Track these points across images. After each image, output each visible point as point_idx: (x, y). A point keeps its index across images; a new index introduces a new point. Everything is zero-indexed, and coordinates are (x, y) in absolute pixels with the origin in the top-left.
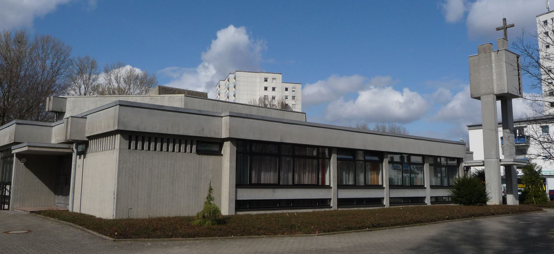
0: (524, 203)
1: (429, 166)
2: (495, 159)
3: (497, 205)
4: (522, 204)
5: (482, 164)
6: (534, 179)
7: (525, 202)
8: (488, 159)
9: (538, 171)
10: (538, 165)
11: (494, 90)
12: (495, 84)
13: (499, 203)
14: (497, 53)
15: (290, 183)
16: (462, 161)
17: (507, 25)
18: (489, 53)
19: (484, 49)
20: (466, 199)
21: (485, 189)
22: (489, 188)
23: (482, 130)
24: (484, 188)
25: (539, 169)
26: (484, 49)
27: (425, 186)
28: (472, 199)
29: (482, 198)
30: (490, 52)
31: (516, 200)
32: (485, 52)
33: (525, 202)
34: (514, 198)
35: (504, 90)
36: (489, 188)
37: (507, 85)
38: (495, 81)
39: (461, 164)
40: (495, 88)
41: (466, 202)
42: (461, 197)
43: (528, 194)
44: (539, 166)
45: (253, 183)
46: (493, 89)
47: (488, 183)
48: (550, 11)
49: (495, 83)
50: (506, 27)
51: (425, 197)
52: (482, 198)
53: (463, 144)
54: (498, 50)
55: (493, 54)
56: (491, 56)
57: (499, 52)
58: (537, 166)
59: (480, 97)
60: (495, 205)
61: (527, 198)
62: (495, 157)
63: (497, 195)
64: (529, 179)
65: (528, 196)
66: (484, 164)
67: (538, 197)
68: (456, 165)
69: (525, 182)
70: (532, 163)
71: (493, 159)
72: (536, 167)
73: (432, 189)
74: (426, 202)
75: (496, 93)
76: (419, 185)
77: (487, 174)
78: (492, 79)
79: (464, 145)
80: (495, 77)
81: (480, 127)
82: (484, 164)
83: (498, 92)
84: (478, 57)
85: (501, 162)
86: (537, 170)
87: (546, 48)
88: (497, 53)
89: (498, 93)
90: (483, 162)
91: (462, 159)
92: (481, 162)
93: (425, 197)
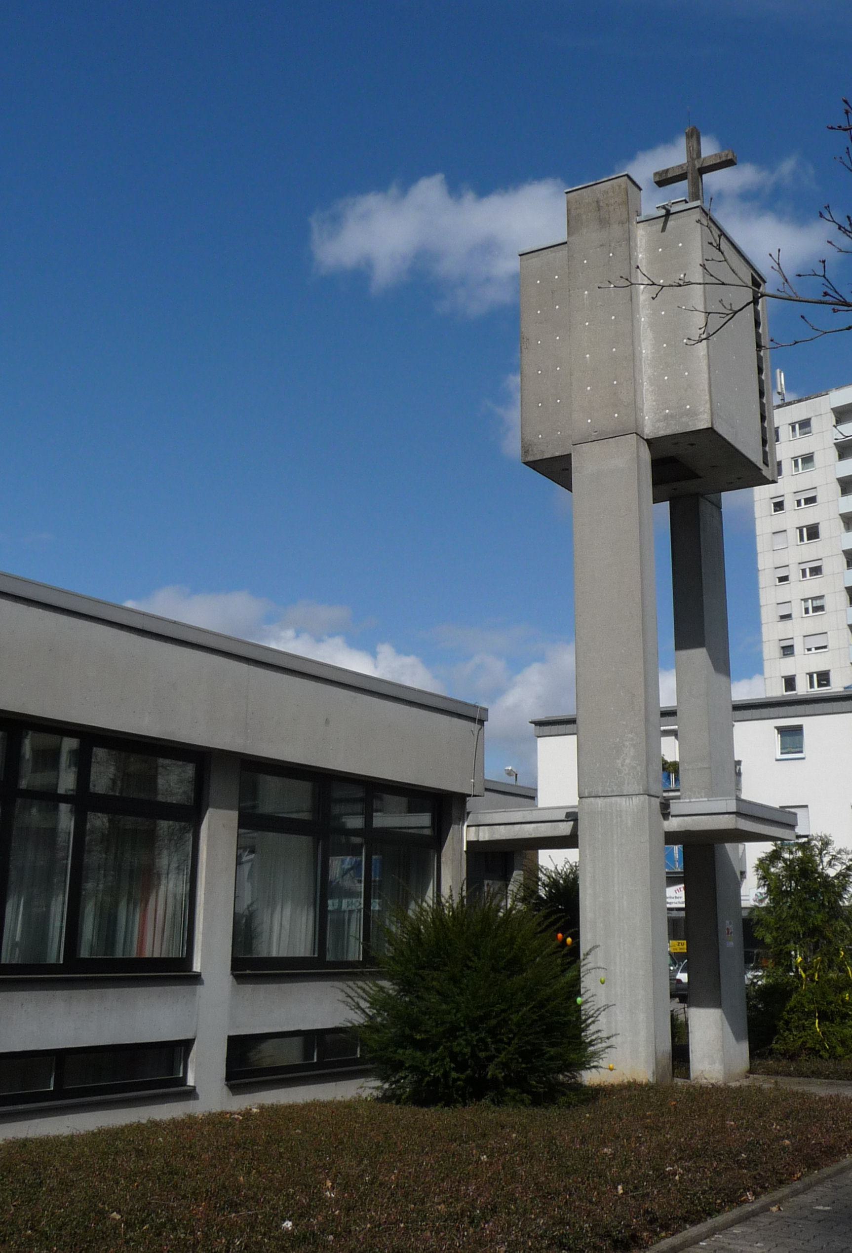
0: (771, 1052)
1: (240, 826)
2: (636, 800)
3: (640, 1085)
4: (761, 1056)
5: (565, 829)
6: (819, 918)
7: (774, 1046)
8: (599, 801)
9: (837, 877)
10: (838, 848)
11: (643, 417)
12: (646, 387)
13: (652, 1067)
14: (664, 229)
15: (55, 953)
16: (463, 815)
17: (703, 156)
18: (622, 223)
19: (599, 208)
20: (453, 1056)
21: (574, 988)
22: (602, 975)
23: (576, 736)
24: (570, 975)
25: (839, 868)
26: (599, 208)
27: (197, 967)
28: (490, 1059)
29: (552, 1051)
30: (629, 220)
31: (738, 1038)
32: (604, 223)
33: (774, 1046)
34: (729, 1030)
35: (693, 414)
36: (602, 975)
37: (707, 389)
38: (647, 372)
39: (454, 828)
40: (646, 407)
41: (454, 1075)
42: (420, 1046)
43: (792, 1003)
44: (839, 852)
45: (82, 956)
46: (635, 406)
47: (595, 947)
48: (786, 401)
49: (645, 378)
50: (698, 166)
51: (186, 1045)
52: (552, 1051)
53: (472, 715)
54: (668, 214)
55: (642, 235)
56: (629, 239)
57: (671, 223)
58: (830, 848)
59: (569, 456)
60: (632, 1086)
61: (787, 1023)
62: (637, 788)
63: (642, 1017)
64: (792, 918)
65: (792, 1010)
66: (575, 829)
67: (838, 1020)
68: (427, 832)
69: (774, 934)
70: (364, 1098)
71: (622, 801)
72: (826, 859)
73: (249, 988)
74: (191, 1082)
75: (649, 431)
76: (156, 955)
77: (589, 891)
78: (633, 357)
79: (473, 719)
80: (646, 349)
81: (570, 727)
82: (575, 829)
83: (661, 424)
84: (565, 252)
85: (666, 815)
86: (832, 872)
87: (775, 511)
88: (664, 229)
89: (662, 433)
90: (572, 817)
91: (462, 798)
92: (563, 817)
93: (186, 1045)
